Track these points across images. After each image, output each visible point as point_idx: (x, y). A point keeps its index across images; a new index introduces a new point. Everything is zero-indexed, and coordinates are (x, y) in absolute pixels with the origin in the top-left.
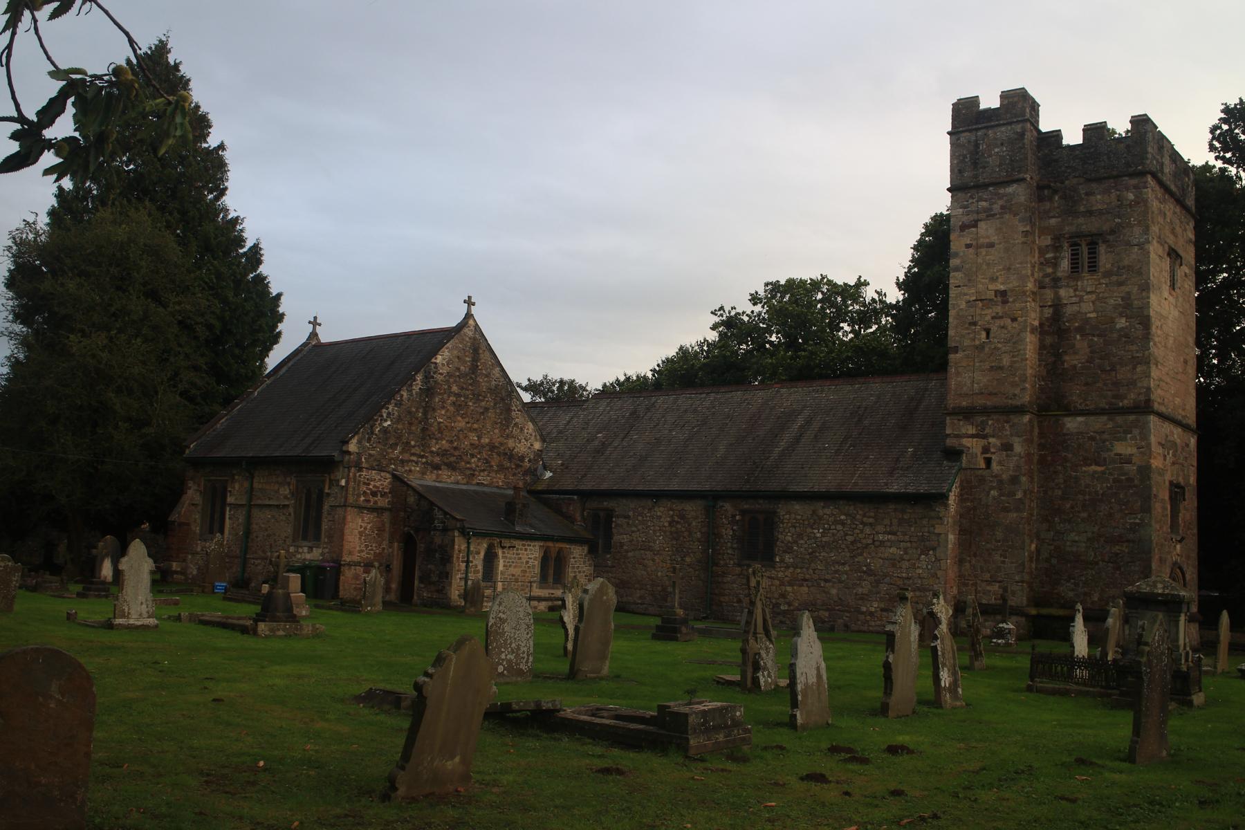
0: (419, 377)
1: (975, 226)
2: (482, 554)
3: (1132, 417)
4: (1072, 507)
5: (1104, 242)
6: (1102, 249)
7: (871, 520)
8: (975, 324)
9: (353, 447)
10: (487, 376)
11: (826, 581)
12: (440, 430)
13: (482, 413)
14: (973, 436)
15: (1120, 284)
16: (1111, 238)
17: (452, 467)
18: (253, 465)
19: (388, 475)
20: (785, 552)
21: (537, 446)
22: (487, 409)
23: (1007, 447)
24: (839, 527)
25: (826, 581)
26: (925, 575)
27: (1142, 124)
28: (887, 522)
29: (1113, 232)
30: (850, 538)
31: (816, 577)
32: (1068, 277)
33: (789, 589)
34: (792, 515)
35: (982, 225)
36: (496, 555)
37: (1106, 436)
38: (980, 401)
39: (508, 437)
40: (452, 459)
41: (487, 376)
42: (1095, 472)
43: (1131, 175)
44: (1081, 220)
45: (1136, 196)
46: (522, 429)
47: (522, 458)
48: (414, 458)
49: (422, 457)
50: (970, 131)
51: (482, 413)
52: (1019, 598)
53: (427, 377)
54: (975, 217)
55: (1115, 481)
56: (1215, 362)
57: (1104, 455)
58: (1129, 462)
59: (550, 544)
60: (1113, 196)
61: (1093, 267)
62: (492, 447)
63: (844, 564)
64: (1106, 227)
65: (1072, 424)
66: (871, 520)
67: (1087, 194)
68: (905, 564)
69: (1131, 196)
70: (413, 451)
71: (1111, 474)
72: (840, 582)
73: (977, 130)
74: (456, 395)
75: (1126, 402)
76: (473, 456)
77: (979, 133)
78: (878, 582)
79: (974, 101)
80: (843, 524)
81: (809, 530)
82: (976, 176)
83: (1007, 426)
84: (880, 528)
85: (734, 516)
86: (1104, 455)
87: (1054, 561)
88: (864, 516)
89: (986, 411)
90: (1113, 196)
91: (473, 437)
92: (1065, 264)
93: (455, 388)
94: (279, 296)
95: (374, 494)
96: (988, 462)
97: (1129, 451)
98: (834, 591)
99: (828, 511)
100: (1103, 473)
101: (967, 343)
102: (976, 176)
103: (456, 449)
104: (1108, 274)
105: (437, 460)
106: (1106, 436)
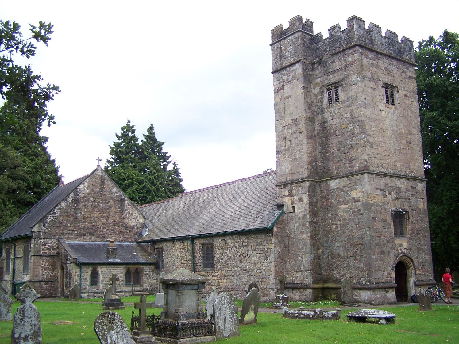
0: (71, 196)
1: (283, 89)
2: (89, 273)
3: (358, 177)
4: (336, 228)
5: (341, 86)
6: (340, 89)
7: (246, 244)
8: (285, 138)
9: (35, 229)
10: (109, 192)
11: (232, 276)
12: (84, 218)
13: (108, 209)
14: (287, 196)
15: (349, 106)
16: (343, 83)
17: (92, 234)
18: (173, 240)
19: (56, 240)
20: (217, 263)
21: (141, 221)
22: (110, 207)
23: (301, 200)
24: (235, 249)
25: (232, 276)
26: (266, 270)
27: (355, 21)
28: (252, 244)
29: (344, 79)
30: (239, 254)
31: (228, 274)
32: (327, 107)
33: (220, 281)
34: (218, 243)
35: (285, 87)
36: (98, 273)
37: (347, 189)
38: (290, 178)
39: (124, 218)
40: (92, 231)
41: (109, 192)
42: (344, 208)
43: (350, 48)
44: (331, 76)
45: (352, 59)
46: (131, 214)
47: (133, 228)
48: (70, 232)
49: (75, 231)
50: (278, 42)
51: (108, 209)
52: (309, 280)
53: (76, 195)
54: (282, 84)
55: (353, 212)
56: (438, 138)
57: (347, 198)
58: (358, 201)
59: (131, 266)
60: (343, 61)
61: (337, 100)
62: (115, 223)
63: (237, 267)
64: (341, 78)
65: (333, 184)
66: (246, 244)
67: (332, 62)
68: (259, 265)
69: (350, 59)
70: (69, 229)
71: (351, 208)
72: (237, 276)
73: (280, 41)
74: (92, 202)
75: (355, 168)
76: (104, 228)
77: (282, 42)
78: (250, 275)
79: (281, 27)
80: (236, 247)
81: (225, 251)
82: (282, 64)
83: (300, 189)
84: (249, 248)
85: (200, 247)
86: (347, 198)
87: (330, 258)
88: (243, 242)
89: (292, 183)
90: (343, 61)
91: (104, 220)
92: (326, 100)
93: (91, 199)
94: (58, 167)
95: (48, 249)
96: (294, 208)
97: (359, 194)
98: (235, 281)
99: (230, 241)
100: (348, 208)
101: (283, 148)
102: (282, 64)
103: (93, 226)
104: (343, 102)
105: (83, 231)
106: (347, 189)
